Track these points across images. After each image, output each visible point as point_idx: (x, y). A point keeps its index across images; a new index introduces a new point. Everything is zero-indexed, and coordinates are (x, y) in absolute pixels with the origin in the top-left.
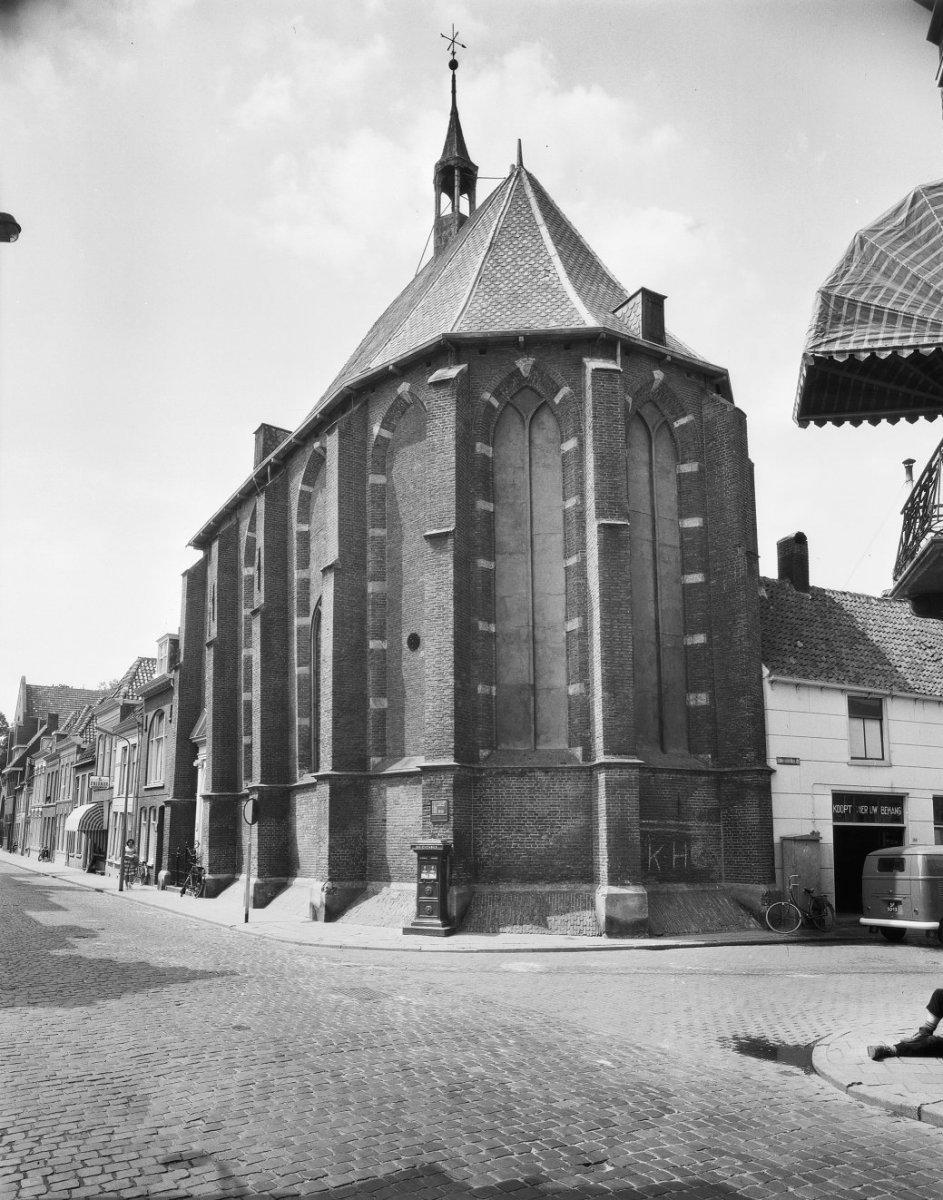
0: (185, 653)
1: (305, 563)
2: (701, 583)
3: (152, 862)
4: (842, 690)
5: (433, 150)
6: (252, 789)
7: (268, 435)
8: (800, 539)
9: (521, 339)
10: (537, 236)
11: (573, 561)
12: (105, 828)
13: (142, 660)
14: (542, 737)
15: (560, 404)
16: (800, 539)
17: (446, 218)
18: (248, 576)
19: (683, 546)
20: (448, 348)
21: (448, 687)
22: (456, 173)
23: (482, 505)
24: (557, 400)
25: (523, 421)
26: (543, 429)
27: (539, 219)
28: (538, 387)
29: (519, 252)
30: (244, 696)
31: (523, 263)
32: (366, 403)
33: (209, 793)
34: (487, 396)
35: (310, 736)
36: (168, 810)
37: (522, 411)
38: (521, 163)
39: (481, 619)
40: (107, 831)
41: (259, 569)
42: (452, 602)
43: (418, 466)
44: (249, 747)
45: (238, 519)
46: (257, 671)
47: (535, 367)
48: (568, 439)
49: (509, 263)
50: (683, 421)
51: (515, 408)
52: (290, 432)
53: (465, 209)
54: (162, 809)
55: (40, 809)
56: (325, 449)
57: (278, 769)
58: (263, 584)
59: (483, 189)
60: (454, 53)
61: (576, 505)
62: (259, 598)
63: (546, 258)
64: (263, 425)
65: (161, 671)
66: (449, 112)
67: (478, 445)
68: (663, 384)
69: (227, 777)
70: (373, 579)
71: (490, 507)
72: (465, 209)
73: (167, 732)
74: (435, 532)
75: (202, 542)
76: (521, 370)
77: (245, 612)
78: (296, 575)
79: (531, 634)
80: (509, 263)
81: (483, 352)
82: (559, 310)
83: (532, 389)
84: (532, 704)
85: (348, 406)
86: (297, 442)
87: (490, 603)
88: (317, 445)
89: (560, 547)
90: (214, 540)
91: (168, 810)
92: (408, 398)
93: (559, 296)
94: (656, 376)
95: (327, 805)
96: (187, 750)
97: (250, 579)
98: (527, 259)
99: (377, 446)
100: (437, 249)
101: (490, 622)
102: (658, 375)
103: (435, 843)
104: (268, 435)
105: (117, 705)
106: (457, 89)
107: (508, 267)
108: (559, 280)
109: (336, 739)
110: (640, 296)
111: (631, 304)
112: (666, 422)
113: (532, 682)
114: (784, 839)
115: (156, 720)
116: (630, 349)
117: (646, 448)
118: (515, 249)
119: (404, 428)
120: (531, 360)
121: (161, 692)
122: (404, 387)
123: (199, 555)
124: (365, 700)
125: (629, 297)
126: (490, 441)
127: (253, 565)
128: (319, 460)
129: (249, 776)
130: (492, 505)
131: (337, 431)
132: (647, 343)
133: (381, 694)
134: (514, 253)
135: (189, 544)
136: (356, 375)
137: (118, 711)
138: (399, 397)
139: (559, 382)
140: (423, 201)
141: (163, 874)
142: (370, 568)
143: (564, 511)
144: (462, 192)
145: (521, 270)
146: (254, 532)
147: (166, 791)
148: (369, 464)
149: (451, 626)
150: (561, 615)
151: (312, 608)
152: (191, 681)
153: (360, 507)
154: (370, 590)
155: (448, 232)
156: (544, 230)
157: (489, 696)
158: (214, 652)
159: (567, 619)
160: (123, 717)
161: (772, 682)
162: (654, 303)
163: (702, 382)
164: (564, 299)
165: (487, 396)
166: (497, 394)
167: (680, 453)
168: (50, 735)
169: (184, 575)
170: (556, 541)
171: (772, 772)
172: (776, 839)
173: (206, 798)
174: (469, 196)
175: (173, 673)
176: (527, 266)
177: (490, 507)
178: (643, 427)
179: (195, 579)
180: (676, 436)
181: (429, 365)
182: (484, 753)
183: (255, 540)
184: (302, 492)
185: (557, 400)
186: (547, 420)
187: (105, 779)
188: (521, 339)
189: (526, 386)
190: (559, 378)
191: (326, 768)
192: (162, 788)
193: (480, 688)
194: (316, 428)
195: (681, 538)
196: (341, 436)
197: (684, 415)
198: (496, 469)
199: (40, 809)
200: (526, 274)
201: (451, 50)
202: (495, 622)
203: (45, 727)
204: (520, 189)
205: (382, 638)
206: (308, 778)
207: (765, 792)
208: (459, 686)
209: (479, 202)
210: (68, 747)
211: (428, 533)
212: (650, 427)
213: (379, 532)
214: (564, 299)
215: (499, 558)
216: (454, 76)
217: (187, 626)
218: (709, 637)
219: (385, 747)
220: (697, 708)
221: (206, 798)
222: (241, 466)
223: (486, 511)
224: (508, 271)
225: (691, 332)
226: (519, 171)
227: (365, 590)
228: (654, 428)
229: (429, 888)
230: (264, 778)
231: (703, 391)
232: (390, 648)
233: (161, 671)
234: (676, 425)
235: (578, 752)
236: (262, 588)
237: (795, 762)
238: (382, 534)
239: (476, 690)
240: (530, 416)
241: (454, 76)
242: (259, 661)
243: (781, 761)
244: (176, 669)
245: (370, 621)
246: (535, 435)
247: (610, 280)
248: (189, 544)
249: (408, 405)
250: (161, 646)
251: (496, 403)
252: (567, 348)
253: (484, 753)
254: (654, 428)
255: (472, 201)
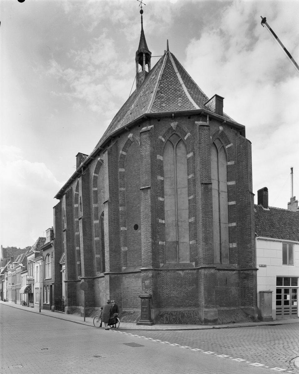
0: (56, 233)
1: (96, 202)
2: (235, 205)
3: (49, 303)
4: (281, 242)
5: (135, 48)
6: (82, 279)
7: (80, 156)
8: (265, 189)
9: (173, 115)
10: (176, 77)
11: (191, 197)
12: (32, 293)
13: (40, 238)
14: (181, 259)
15: (186, 140)
16: (265, 189)
17: (140, 73)
18: (76, 207)
19: (228, 192)
20: (147, 119)
21: (149, 242)
22: (143, 56)
23: (160, 178)
24: (185, 138)
25: (173, 146)
26: (180, 149)
27: (176, 70)
28: (179, 134)
29: (170, 83)
30: (77, 248)
31: (171, 87)
32: (117, 142)
33: (66, 280)
34: (160, 137)
35: (100, 261)
36: (53, 286)
37: (173, 143)
38: (168, 50)
39: (160, 219)
40: (33, 294)
41: (81, 204)
42: (150, 213)
43: (136, 165)
44: (80, 265)
45: (72, 188)
46: (81, 239)
47: (178, 126)
48: (189, 153)
49: (166, 87)
50: (229, 146)
51: (171, 142)
52: (87, 156)
53: (147, 70)
54: (51, 286)
55: (11, 287)
56: (102, 161)
57: (90, 272)
58: (66, 221)
59: (154, 61)
60: (141, 7)
61: (193, 177)
62: (81, 214)
63: (180, 85)
64: (79, 153)
65: (48, 241)
66: (141, 31)
67: (158, 156)
68: (222, 132)
69: (72, 276)
70: (121, 206)
71: (162, 178)
72: (147, 70)
73: (51, 261)
74: (144, 187)
75: (59, 196)
76: (173, 127)
77: (76, 220)
78: (94, 206)
79: (177, 224)
80: (166, 87)
81: (159, 121)
82: (186, 104)
83: (177, 135)
84: (178, 248)
85: (109, 142)
86: (78, 173)
87: (163, 213)
88: (99, 159)
89: (187, 192)
90: (64, 194)
91: (53, 286)
92: (132, 140)
93: (185, 99)
94: (220, 129)
95: (109, 283)
96: (58, 267)
97: (77, 208)
98: (173, 85)
99: (121, 158)
100: (137, 85)
101: (163, 220)
102: (221, 128)
103: (146, 295)
104: (80, 156)
105: (34, 253)
106: (143, 22)
107: (166, 89)
108: (185, 93)
109: (110, 261)
110: (215, 97)
111: (211, 101)
112: (223, 146)
113: (177, 240)
114: (260, 292)
115: (47, 257)
116: (212, 118)
117: (216, 156)
118: (168, 82)
119: (131, 151)
120: (176, 123)
121: (49, 246)
122: (130, 135)
123: (59, 201)
124: (120, 247)
125: (210, 99)
126: (162, 155)
127: (77, 203)
128: (100, 164)
129: (80, 274)
130: (163, 178)
131: (81, 177)
132: (216, 115)
133: (125, 246)
134: (168, 83)
135: (55, 197)
136: (109, 135)
137: (34, 255)
138: (129, 139)
139: (186, 131)
140: (130, 67)
141: (53, 307)
142: (120, 202)
143: (188, 179)
144: (146, 64)
145: (171, 90)
146: (78, 191)
147: (52, 280)
148: (119, 165)
149: (150, 221)
150: (187, 216)
151: (99, 217)
152: (57, 243)
153: (116, 180)
154: (120, 210)
155: (142, 79)
156: (178, 74)
157: (163, 245)
158: (66, 233)
159: (189, 218)
160: (36, 257)
161: (258, 239)
162: (219, 100)
163: (236, 131)
164: (187, 100)
165: (160, 137)
166: (164, 137)
167: (228, 158)
168: (12, 263)
169: (53, 208)
170: (185, 191)
171: (257, 269)
172: (258, 291)
173: (65, 282)
174: (148, 65)
175: (52, 241)
176: (173, 88)
177: (162, 178)
178: (215, 148)
179: (57, 209)
180: (227, 151)
181: (139, 126)
182: (162, 265)
183: (78, 194)
184: (94, 176)
185: (185, 138)
186: (181, 145)
187: (31, 277)
188: (173, 115)
189: (174, 134)
190: (186, 130)
191: (108, 270)
192: (51, 279)
193: (160, 243)
194: (98, 152)
195: (228, 189)
196: (109, 154)
197: (230, 144)
198: (164, 165)
199: (11, 287)
200: (173, 91)
201: (140, 6)
202: (164, 220)
203: (10, 261)
204: (168, 61)
205: (125, 226)
206: (102, 274)
207: (254, 277)
208: (153, 242)
209: (152, 67)
210: (18, 267)
211: (141, 188)
212: (218, 148)
213: (122, 189)
214: (187, 100)
215: (165, 197)
216: (142, 16)
217: (56, 225)
218: (237, 224)
219: (127, 264)
220: (232, 248)
221: (65, 282)
222: (72, 169)
223: (161, 180)
224: (166, 90)
225: (232, 111)
226: (167, 53)
227: (119, 210)
228: (219, 148)
229: (145, 310)
230: (86, 275)
231: (236, 134)
232: (128, 229)
233: (48, 241)
234: (227, 147)
235: (194, 264)
236: (82, 210)
237: (265, 266)
238: (124, 190)
239: (158, 243)
240: (176, 145)
241: (142, 16)
242: (82, 236)
243: (261, 266)
244: (53, 240)
245: (121, 221)
246: (177, 152)
247: (202, 94)
248: (55, 197)
249: (132, 142)
250: (47, 232)
251: (164, 140)
252: (189, 118)
253: (162, 265)
254: (219, 148)
255: (149, 67)
